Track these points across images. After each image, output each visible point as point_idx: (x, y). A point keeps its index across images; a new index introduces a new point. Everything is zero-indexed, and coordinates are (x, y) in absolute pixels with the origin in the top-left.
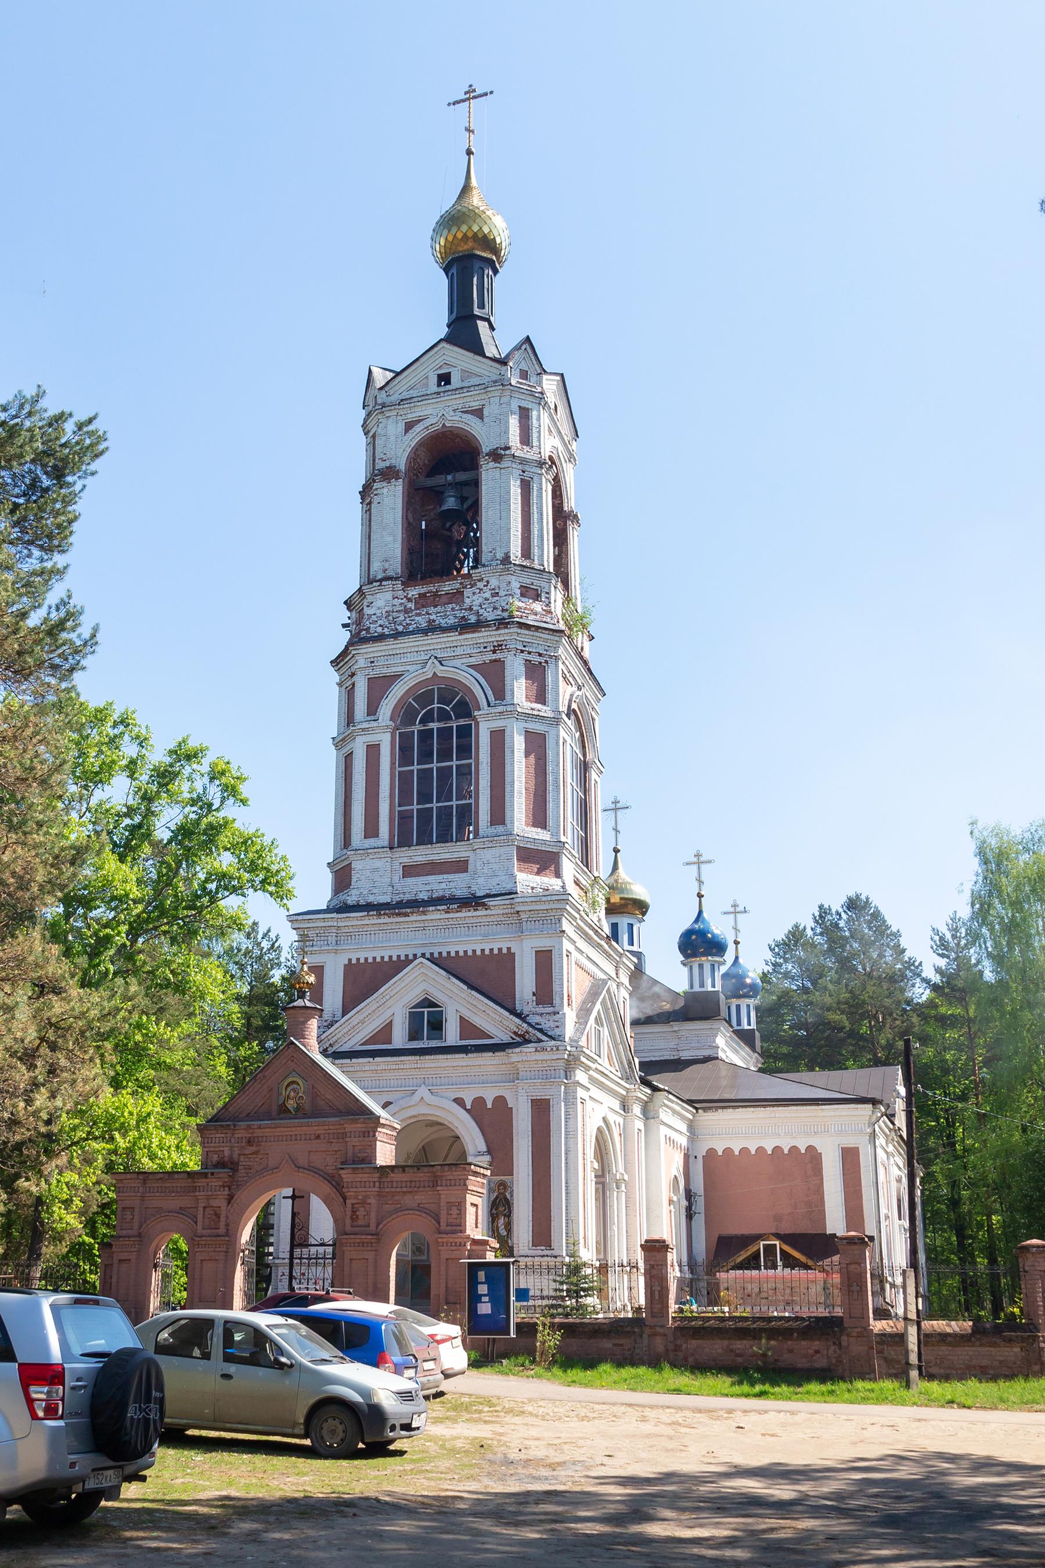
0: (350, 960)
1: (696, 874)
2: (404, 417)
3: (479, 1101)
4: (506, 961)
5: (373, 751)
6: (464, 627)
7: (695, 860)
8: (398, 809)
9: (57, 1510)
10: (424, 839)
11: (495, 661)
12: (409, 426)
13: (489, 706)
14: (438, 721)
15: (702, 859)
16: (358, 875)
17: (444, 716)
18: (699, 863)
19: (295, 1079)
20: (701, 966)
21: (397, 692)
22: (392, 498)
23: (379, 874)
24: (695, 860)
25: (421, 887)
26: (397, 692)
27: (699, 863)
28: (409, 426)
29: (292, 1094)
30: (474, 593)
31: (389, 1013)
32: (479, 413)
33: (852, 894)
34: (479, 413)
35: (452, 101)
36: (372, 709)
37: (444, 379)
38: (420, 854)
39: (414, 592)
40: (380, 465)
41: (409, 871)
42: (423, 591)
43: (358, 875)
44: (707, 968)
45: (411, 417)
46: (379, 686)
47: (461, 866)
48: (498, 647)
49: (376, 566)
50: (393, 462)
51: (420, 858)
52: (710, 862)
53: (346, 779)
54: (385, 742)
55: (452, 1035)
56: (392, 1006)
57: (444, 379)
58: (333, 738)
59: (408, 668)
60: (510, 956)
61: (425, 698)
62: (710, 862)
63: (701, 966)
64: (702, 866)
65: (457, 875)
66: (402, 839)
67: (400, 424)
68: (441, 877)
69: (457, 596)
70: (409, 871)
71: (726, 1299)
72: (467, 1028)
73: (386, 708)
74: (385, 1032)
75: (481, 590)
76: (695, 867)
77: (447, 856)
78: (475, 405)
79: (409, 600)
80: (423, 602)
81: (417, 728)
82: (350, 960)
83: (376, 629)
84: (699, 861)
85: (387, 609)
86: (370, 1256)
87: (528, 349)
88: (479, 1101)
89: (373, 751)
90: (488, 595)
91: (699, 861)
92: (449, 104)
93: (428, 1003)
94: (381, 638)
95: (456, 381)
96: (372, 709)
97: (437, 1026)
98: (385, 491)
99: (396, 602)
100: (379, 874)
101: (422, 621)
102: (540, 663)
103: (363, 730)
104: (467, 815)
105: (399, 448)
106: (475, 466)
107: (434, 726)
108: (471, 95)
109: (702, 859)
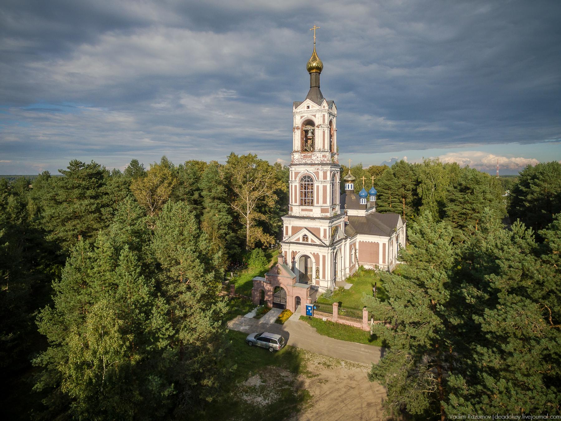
3: (314, 253)
4: (319, 230)
5: (296, 186)
6: (312, 164)
9: (559, 391)
12: (301, 117)
17: (308, 181)
21: (299, 175)
26: (299, 175)
32: (315, 116)
34: (315, 116)
36: (295, 178)
38: (304, 207)
39: (303, 155)
41: (302, 210)
45: (302, 115)
48: (318, 169)
54: (298, 185)
56: (300, 235)
60: (320, 229)
61: (305, 177)
69: (310, 157)
70: (302, 210)
71: (557, 276)
72: (312, 241)
73: (298, 179)
74: (299, 239)
78: (314, 114)
81: (303, 183)
83: (296, 162)
86: (328, 243)
88: (314, 253)
89: (296, 186)
93: (305, 235)
94: (296, 165)
96: (295, 178)
101: (304, 161)
104: (312, 203)
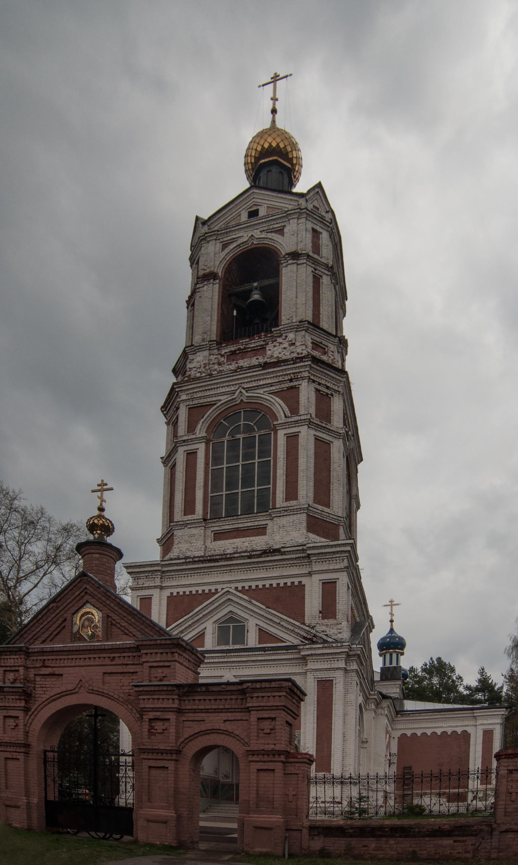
0: (172, 593)
1: (389, 611)
2: (221, 240)
5: (191, 455)
7: (390, 604)
8: (210, 495)
10: (231, 513)
11: (292, 388)
13: (286, 417)
14: (244, 433)
15: (393, 603)
16: (178, 540)
18: (392, 605)
19: (88, 610)
20: (391, 655)
22: (212, 293)
23: (193, 542)
24: (390, 604)
25: (228, 546)
26: (210, 414)
27: (392, 605)
28: (225, 246)
29: (87, 623)
30: (275, 346)
31: (202, 627)
33: (440, 656)
35: (261, 84)
37: (253, 214)
38: (227, 525)
40: (201, 273)
42: (233, 349)
43: (178, 540)
44: (394, 656)
46: (196, 411)
47: (261, 531)
49: (197, 339)
50: (212, 269)
51: (227, 527)
52: (398, 604)
53: (171, 484)
55: (252, 640)
57: (253, 214)
58: (162, 458)
59: (220, 398)
62: (398, 604)
63: (391, 655)
64: (394, 607)
65: (257, 537)
66: (212, 515)
67: (218, 245)
68: (244, 539)
70: (218, 536)
75: (281, 343)
76: (389, 607)
77: (250, 524)
79: (222, 356)
80: (233, 356)
82: (172, 593)
84: (392, 604)
85: (205, 362)
87: (320, 191)
89: (191, 455)
90: (286, 345)
91: (392, 604)
92: (259, 86)
95: (262, 212)
97: (240, 632)
98: (206, 287)
99: (212, 357)
100: (193, 542)
102: (327, 394)
103: (184, 441)
105: (216, 258)
106: (276, 274)
107: (241, 436)
108: (276, 78)
109: (393, 603)
